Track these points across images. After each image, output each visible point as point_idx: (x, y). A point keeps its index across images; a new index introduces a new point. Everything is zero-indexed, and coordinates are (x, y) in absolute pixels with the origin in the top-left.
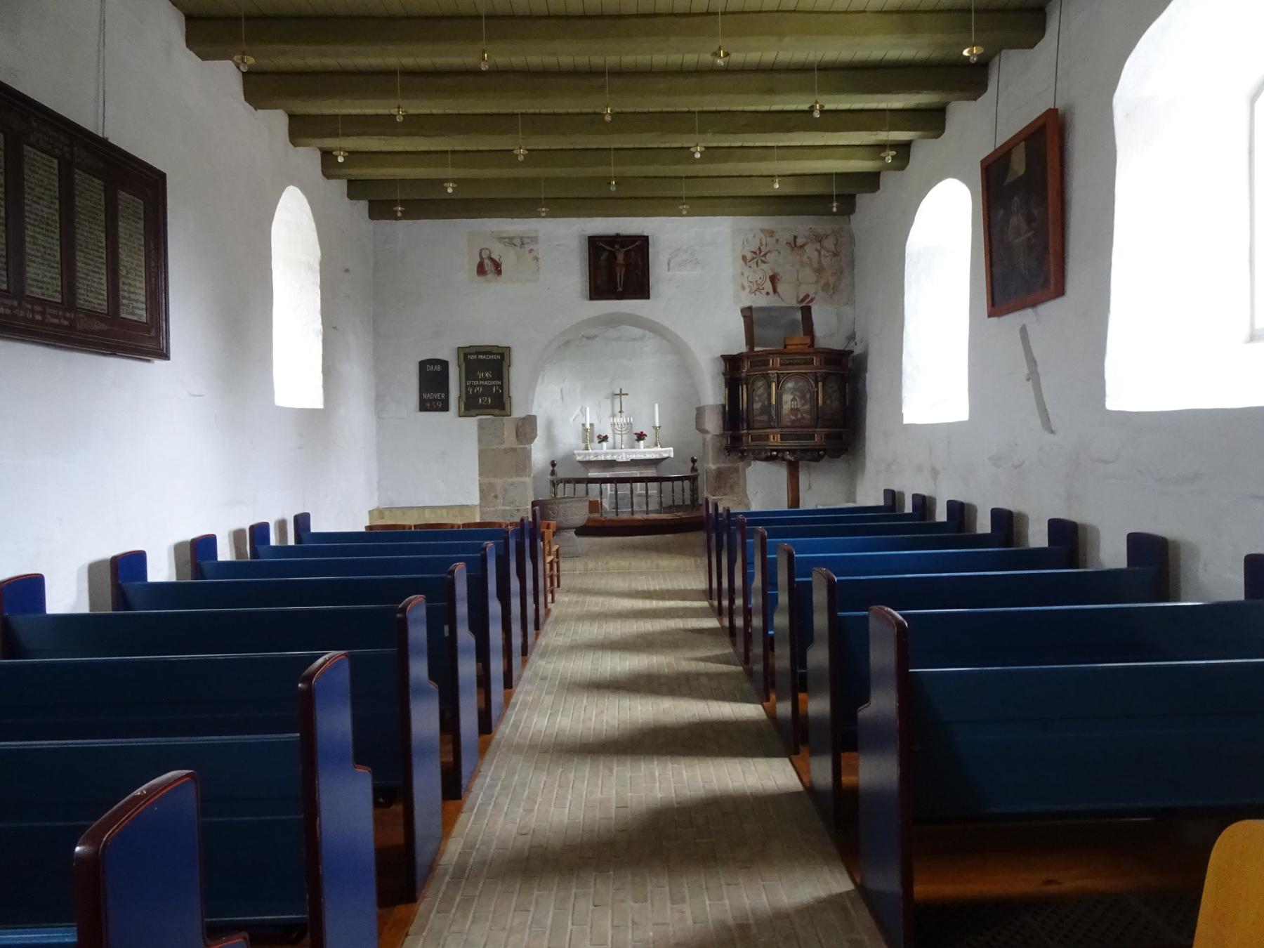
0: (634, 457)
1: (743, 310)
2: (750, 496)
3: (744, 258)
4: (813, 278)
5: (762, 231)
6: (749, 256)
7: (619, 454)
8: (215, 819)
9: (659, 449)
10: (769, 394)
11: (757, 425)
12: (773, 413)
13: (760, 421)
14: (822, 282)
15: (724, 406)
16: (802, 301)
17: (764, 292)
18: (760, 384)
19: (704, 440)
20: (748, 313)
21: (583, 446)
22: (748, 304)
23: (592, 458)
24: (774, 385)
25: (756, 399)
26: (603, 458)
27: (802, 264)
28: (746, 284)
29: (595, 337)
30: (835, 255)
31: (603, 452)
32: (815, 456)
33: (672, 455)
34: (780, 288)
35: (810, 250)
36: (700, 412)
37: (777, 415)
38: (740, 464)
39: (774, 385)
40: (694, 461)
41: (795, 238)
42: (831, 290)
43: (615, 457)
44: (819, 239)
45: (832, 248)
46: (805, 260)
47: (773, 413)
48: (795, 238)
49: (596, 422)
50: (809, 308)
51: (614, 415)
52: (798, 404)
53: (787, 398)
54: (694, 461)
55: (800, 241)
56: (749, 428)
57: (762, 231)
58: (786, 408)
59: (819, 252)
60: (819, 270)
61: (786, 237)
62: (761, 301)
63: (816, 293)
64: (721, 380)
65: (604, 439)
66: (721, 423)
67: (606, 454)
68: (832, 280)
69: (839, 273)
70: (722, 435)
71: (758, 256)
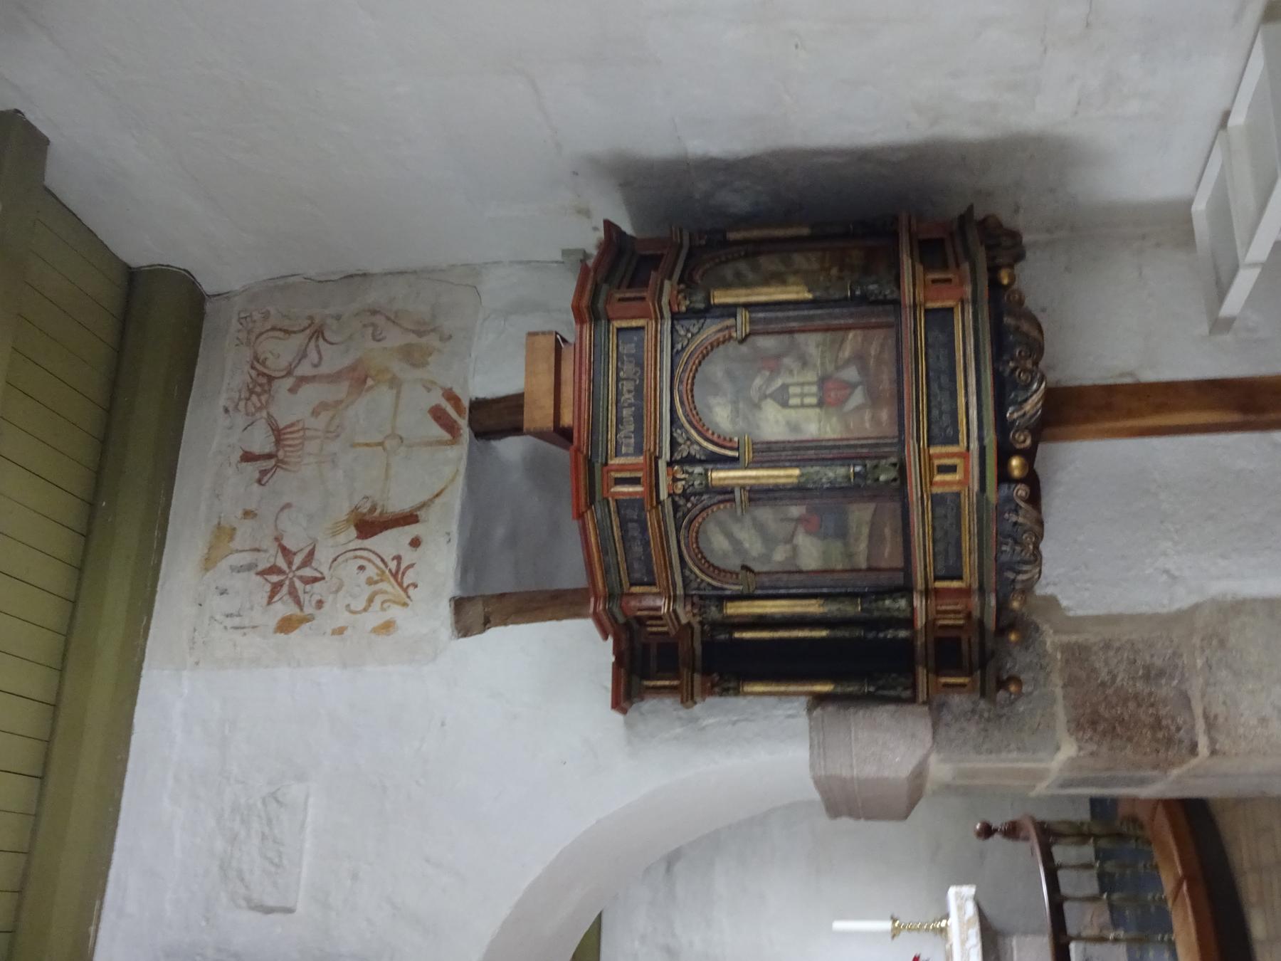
1: (464, 629)
2: (1183, 599)
3: (286, 625)
4: (384, 395)
5: (209, 563)
6: (283, 608)
9: (953, 923)
10: (760, 495)
11: (890, 555)
12: (836, 473)
13: (875, 538)
14: (397, 367)
15: (819, 700)
16: (451, 427)
17: (409, 556)
18: (717, 543)
19: (947, 789)
20: (478, 610)
22: (445, 611)
24: (720, 476)
25: (774, 551)
27: (332, 433)
28: (375, 618)
30: (319, 333)
32: (1014, 338)
33: (969, 891)
34: (398, 504)
35: (292, 407)
36: (845, 802)
37: (846, 460)
38: (1051, 639)
39: (720, 476)
40: (987, 831)
41: (248, 457)
42: (425, 337)
44: (262, 382)
45: (297, 341)
46: (320, 423)
47: (836, 473)
48: (248, 457)
50: (478, 406)
52: (802, 384)
53: (774, 424)
54: (987, 831)
55: (261, 441)
56: (906, 590)
57: (209, 563)
58: (816, 426)
59: (303, 380)
60: (359, 378)
61: (239, 486)
62: (439, 566)
63: (428, 386)
64: (715, 712)
66: (884, 714)
68: (395, 339)
69: (376, 318)
70: (937, 710)
71: (289, 581)
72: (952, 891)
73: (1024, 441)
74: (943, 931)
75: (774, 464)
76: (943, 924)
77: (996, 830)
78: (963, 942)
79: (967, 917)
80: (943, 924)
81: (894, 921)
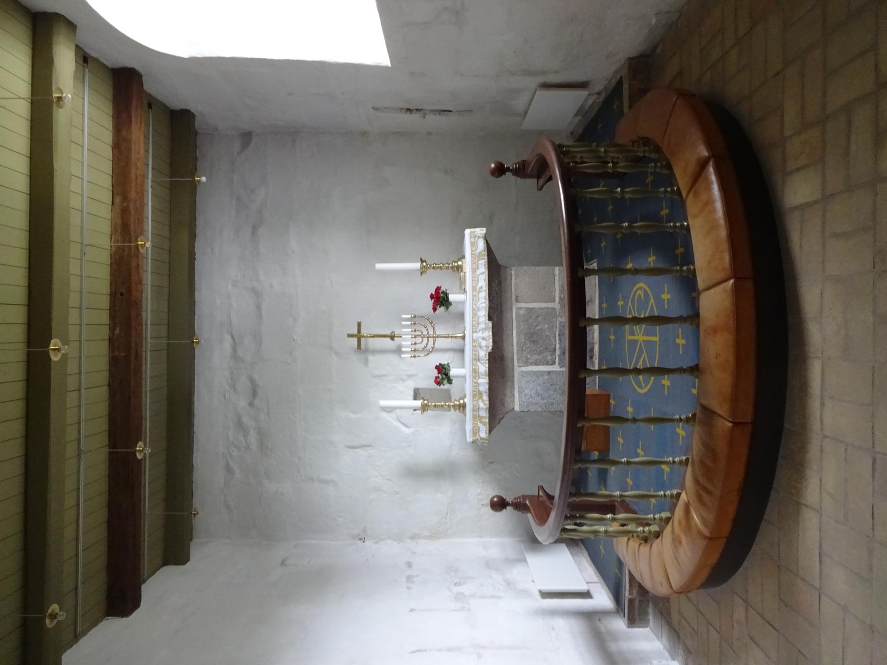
0: (483, 314)
7: (476, 346)
8: (515, 324)
9: (467, 264)
21: (454, 414)
23: (484, 404)
26: (484, 381)
29: (252, 380)
31: (471, 375)
33: (481, 231)
40: (500, 170)
43: (483, 354)
49: (411, 385)
51: (398, 351)
54: (500, 170)
65: (443, 372)
67: (475, 372)
72: (467, 232)
73: (640, 288)
74: (459, 268)
75: (148, 152)
76: (460, 263)
77: (508, 169)
78: (474, 271)
79: (478, 251)
80: (460, 263)
81: (422, 261)
